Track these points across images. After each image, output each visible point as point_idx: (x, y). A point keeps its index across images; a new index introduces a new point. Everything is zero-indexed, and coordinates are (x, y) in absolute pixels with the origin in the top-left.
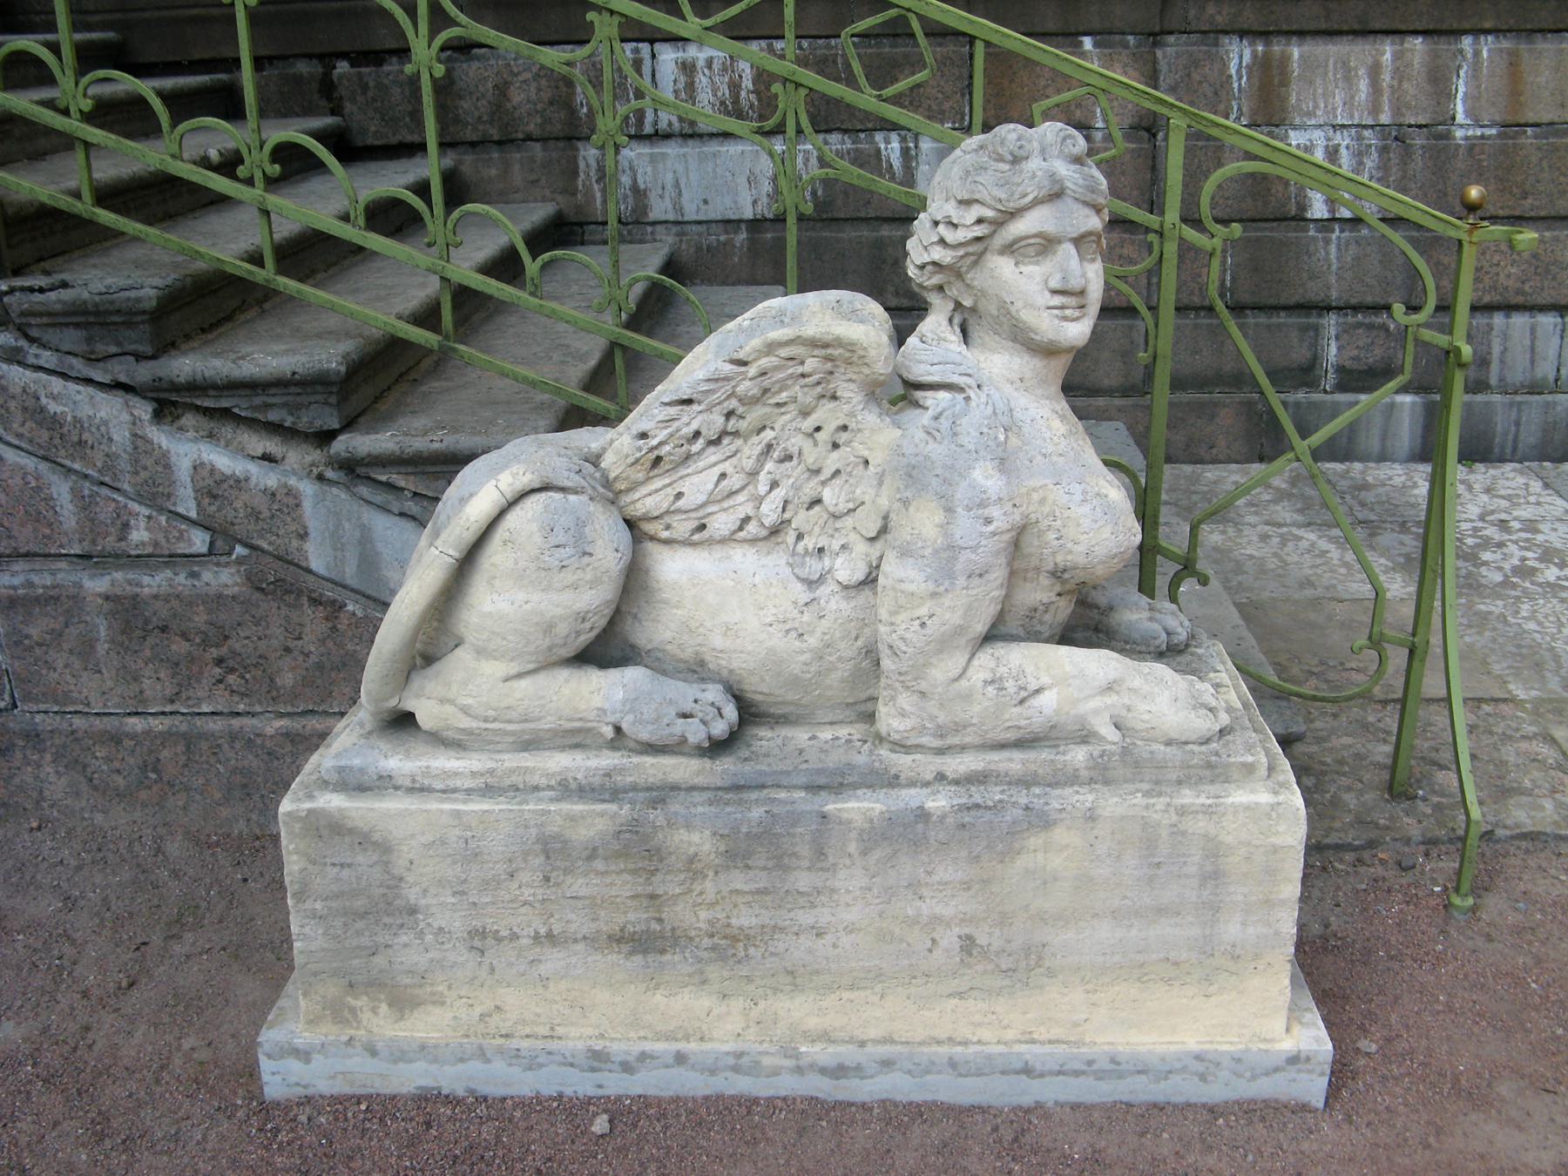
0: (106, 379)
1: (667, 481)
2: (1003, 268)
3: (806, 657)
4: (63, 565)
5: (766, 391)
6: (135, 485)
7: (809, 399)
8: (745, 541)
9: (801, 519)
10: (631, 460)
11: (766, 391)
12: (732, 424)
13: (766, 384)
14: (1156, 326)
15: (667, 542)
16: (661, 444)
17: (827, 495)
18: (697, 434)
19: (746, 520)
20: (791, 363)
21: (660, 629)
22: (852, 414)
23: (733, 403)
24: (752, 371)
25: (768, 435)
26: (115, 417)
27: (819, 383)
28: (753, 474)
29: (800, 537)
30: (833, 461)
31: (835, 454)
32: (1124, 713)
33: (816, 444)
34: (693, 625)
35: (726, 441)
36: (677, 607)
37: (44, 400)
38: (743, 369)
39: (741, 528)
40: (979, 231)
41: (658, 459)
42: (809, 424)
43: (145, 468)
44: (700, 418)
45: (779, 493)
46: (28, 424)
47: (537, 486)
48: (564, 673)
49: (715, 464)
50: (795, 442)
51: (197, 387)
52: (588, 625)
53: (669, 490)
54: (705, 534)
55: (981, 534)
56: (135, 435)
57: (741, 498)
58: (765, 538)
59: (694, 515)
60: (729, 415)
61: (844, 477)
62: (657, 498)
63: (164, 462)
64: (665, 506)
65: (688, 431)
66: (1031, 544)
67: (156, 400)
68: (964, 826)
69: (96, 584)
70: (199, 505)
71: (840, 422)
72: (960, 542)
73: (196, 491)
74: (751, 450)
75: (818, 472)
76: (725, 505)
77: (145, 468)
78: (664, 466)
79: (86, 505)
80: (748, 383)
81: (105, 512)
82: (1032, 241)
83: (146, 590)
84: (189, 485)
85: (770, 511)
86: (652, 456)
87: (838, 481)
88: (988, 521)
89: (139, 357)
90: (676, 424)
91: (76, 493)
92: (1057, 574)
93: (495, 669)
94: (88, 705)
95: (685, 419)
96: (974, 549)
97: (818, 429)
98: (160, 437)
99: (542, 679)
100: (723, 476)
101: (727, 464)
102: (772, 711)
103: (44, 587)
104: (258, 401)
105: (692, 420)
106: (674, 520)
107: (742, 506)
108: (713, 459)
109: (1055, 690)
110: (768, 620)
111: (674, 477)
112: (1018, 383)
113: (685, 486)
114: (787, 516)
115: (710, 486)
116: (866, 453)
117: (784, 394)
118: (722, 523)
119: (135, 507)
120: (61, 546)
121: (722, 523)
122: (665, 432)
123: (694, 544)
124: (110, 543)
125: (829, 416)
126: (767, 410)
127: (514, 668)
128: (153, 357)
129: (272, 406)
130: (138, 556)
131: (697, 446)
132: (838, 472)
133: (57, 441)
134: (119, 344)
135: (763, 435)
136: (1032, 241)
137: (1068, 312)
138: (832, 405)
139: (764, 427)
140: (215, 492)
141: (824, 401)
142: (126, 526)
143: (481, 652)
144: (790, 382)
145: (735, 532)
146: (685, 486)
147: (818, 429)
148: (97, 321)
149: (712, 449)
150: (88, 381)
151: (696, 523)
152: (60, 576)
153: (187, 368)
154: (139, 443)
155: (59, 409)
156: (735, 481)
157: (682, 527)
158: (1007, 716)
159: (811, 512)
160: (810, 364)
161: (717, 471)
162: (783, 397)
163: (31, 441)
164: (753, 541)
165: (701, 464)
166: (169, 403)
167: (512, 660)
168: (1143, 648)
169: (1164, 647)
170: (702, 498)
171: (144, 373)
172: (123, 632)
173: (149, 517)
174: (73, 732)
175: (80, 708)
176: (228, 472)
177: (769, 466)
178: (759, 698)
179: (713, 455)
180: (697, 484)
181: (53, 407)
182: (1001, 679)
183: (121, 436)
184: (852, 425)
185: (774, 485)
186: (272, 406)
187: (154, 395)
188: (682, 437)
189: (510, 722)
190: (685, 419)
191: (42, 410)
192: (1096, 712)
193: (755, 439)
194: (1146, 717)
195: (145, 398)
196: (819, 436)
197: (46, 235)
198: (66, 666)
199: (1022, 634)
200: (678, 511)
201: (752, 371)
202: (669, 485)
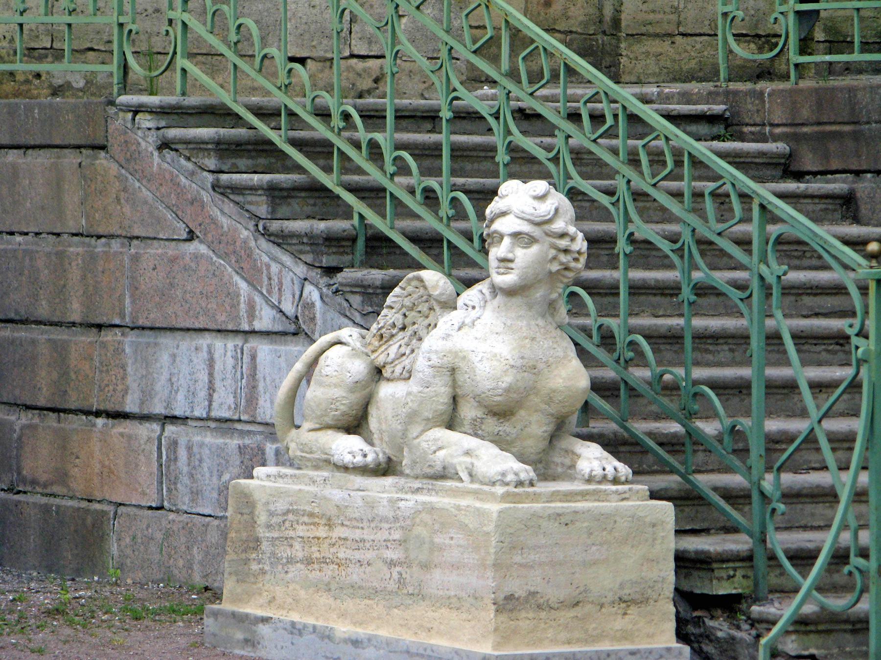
23: (404, 310)
60: (405, 315)
78: (384, 339)
92: (480, 401)
99: (320, 434)
149: (401, 333)
169: (587, 476)
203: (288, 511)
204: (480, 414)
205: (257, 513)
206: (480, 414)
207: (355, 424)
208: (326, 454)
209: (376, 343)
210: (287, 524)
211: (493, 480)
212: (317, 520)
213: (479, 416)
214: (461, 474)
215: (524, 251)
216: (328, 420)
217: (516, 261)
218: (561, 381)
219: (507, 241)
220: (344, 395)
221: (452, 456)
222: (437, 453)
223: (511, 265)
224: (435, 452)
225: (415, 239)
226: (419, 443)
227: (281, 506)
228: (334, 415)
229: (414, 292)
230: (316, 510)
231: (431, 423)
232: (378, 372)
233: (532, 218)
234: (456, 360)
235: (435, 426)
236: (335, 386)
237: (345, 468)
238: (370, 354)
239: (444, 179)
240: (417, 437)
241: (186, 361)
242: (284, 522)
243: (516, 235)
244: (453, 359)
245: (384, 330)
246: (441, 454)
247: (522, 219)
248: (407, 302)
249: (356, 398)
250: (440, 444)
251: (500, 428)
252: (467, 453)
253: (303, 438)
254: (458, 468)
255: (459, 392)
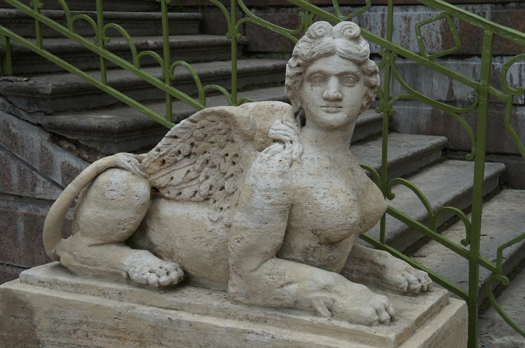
0: (35, 121)
1: (168, 171)
2: (307, 87)
3: (208, 255)
4: (12, 198)
5: (206, 136)
6: (40, 167)
7: (222, 141)
8: (194, 202)
9: (217, 194)
10: (152, 160)
11: (206, 136)
12: (194, 150)
13: (205, 132)
14: (475, 133)
15: (169, 199)
16: (164, 154)
17: (227, 184)
18: (179, 152)
19: (196, 192)
20: (214, 124)
21: (155, 235)
22: (239, 150)
23: (192, 140)
24: (198, 125)
25: (207, 155)
26: (35, 139)
27: (225, 134)
28: (199, 172)
29: (215, 202)
30: (231, 170)
31: (233, 167)
32: (331, 302)
33: (225, 162)
34: (171, 235)
35: (192, 157)
36: (166, 227)
37: (10, 127)
38: (194, 124)
39: (194, 195)
40: (298, 70)
41: (164, 162)
42: (223, 152)
43: (45, 161)
44: (181, 144)
45: (209, 181)
46: (4, 136)
47: (113, 166)
48: (114, 247)
49: (187, 166)
50: (217, 161)
51: (65, 128)
52: (121, 227)
53: (168, 175)
54: (181, 196)
55: (265, 204)
56: (42, 146)
57: (194, 182)
58: (202, 201)
59: (177, 188)
60: (192, 144)
61: (234, 177)
62: (164, 178)
63: (51, 159)
64: (166, 182)
65: (175, 150)
66: (297, 213)
67: (50, 132)
68: (246, 341)
69: (23, 210)
70: (63, 179)
71: (235, 153)
72: (256, 206)
73: (62, 173)
74: (201, 159)
75: (225, 174)
76: (189, 185)
77: (45, 161)
78: (166, 165)
79: (22, 174)
80: (197, 131)
81: (29, 180)
82: (317, 75)
83: (40, 214)
84: (60, 170)
85: (204, 189)
86: (161, 159)
87: (231, 179)
88: (269, 198)
89: (46, 114)
90: (171, 146)
91: (19, 169)
92: (314, 232)
93: (87, 241)
94: (14, 262)
95: (174, 144)
96: (262, 210)
97: (227, 155)
98: (51, 148)
99: (104, 248)
100: (189, 171)
101: (191, 166)
102: (201, 281)
103: (4, 207)
104: (88, 138)
105: (176, 145)
106: (170, 189)
107: (194, 186)
108: (186, 164)
109: (297, 285)
110: (194, 236)
111: (170, 170)
112: (314, 143)
113: (174, 175)
114: (211, 192)
115: (183, 175)
116: (242, 167)
117: (213, 138)
118: (187, 192)
119: (40, 177)
120: (11, 190)
121: (187, 192)
122: (166, 149)
123: (177, 201)
124: (26, 194)
125: (229, 149)
126: (207, 144)
127: (93, 241)
128: (51, 114)
129: (93, 141)
130: (39, 199)
131: (179, 158)
132: (232, 175)
133: (14, 145)
134: (39, 107)
135: (205, 155)
136: (317, 75)
137: (329, 109)
138: (231, 145)
139: (205, 152)
140: (69, 174)
141: (229, 143)
142: (35, 185)
143: (84, 234)
144: (215, 132)
145: (191, 197)
146: (174, 175)
147: (227, 155)
148: (32, 96)
149: (186, 159)
150: (28, 121)
151: (178, 191)
152: (10, 203)
153: (61, 120)
154: (43, 149)
155: (16, 131)
156: (192, 175)
157: (173, 193)
158: (274, 293)
159: (221, 192)
160: (221, 125)
161: (186, 169)
162: (213, 139)
163: (4, 143)
164: (197, 202)
165: (181, 166)
166: (57, 136)
167: (92, 238)
168: (395, 289)
169: (405, 289)
170: (180, 180)
171: (45, 120)
172: (30, 231)
173: (44, 182)
174: (5, 273)
175: (11, 263)
176: (75, 166)
177: (206, 169)
178: (193, 273)
179: (186, 162)
180: (179, 174)
181: (13, 130)
182: (273, 274)
183: (37, 145)
184: (239, 155)
185: (207, 178)
186: (93, 141)
187: (50, 130)
188: (173, 152)
189: (89, 265)
190: (174, 144)
191: (10, 131)
192: (317, 299)
193: (201, 157)
194: (340, 306)
195: (47, 131)
196: (227, 158)
197: (26, 62)
198: (7, 243)
199: (303, 260)
200: (171, 185)
201: (198, 125)
202: (169, 173)
203: (81, 322)
204: (314, 244)
205: (36, 319)
206: (314, 244)
207: (136, 238)
208: (115, 268)
209: (157, 168)
210: (79, 333)
211: (370, 320)
212: (121, 335)
213: (312, 245)
214: (320, 309)
215: (350, 89)
216: (114, 238)
217: (345, 99)
218: (373, 204)
219: (333, 82)
220: (132, 216)
221: (306, 292)
222: (286, 288)
223: (339, 104)
224: (282, 286)
225: (60, 52)
226: (260, 276)
227: (71, 316)
228: (121, 234)
229: (208, 125)
230: (121, 327)
231: (266, 257)
232: (156, 193)
233: (355, 57)
234: (295, 197)
235: (270, 258)
236: (124, 208)
237: (145, 285)
238: (148, 176)
239: (97, 12)
240: (255, 270)
241: (262, 337)
242: (75, 331)
243: (342, 76)
244: (293, 196)
245: (167, 156)
246: (293, 288)
247: (345, 58)
248: (198, 133)
249: (139, 218)
250: (287, 278)
251: (331, 254)
252: (325, 288)
253: (77, 247)
254: (315, 303)
255: (294, 224)
